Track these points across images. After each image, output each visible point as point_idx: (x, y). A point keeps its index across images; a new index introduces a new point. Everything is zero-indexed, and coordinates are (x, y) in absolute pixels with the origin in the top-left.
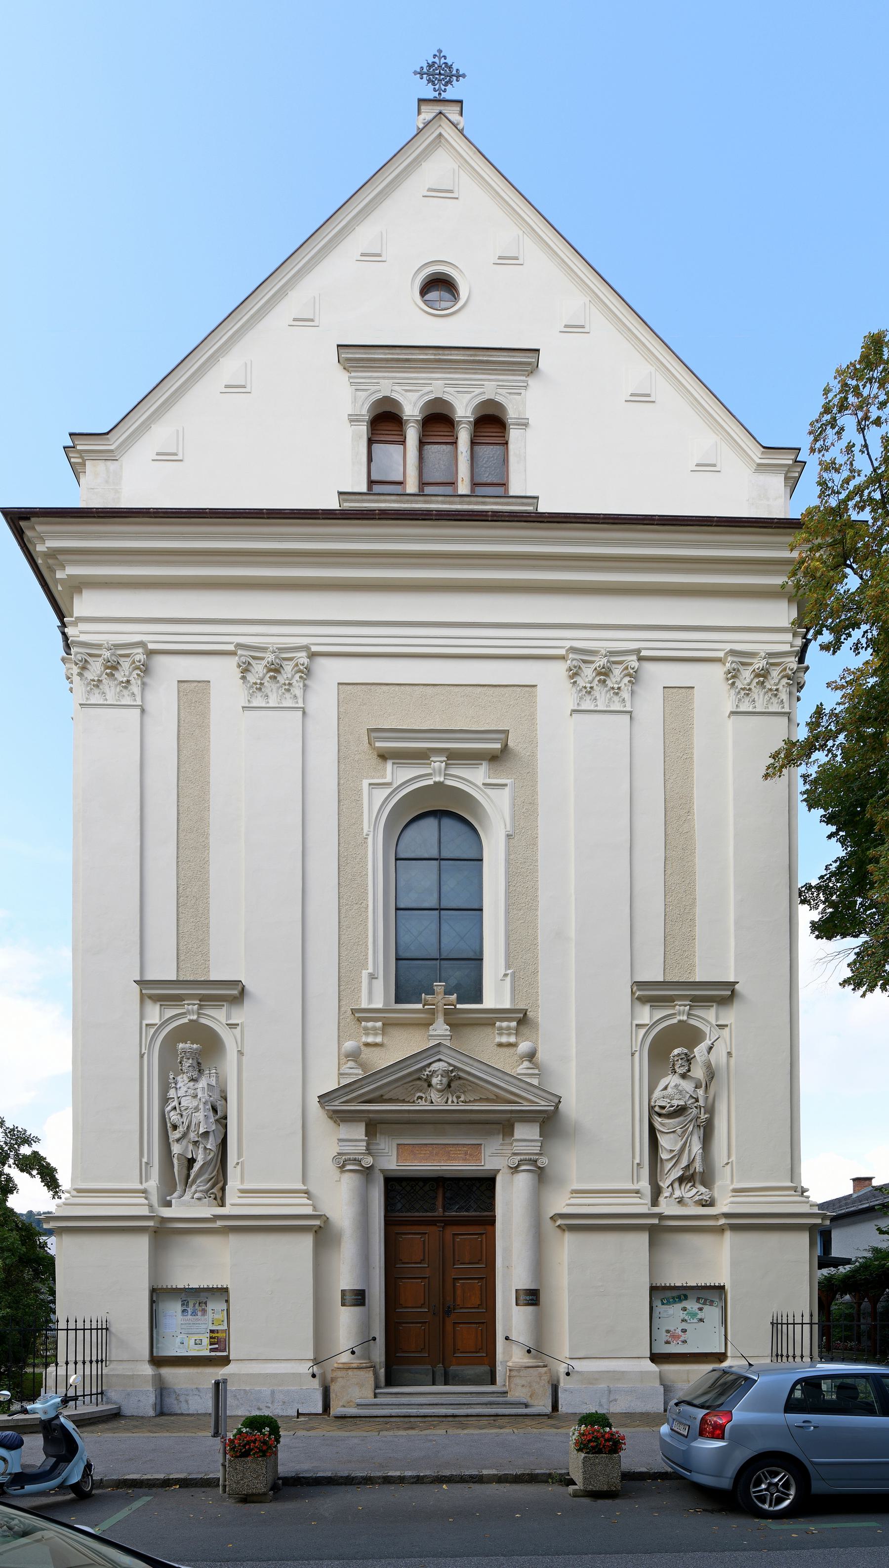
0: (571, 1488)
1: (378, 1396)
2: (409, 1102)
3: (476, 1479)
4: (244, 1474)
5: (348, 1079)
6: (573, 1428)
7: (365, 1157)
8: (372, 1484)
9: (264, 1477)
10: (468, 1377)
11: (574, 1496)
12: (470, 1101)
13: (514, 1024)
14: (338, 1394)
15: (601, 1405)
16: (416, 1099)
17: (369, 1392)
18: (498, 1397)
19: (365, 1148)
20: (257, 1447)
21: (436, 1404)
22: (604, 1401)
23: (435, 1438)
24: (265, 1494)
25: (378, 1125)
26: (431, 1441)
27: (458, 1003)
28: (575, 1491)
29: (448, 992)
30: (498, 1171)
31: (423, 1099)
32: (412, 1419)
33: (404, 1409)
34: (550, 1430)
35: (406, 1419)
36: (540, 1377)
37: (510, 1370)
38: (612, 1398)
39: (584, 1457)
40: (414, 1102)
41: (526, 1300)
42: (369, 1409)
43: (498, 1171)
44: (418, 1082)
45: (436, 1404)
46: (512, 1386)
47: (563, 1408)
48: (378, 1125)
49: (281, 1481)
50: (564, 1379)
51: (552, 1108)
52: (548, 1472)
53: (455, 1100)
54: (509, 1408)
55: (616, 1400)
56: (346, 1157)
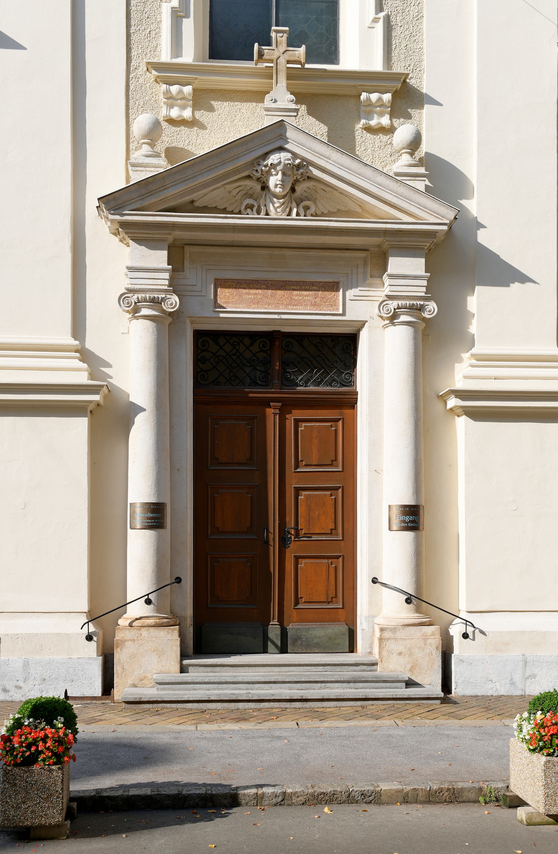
0: (521, 813)
1: (190, 669)
2: (232, 212)
3: (371, 798)
4: (27, 793)
5: (143, 173)
6: (518, 716)
7: (168, 296)
8: (214, 807)
9: (58, 797)
10: (316, 641)
11: (529, 824)
12: (323, 215)
13: (387, 97)
14: (126, 667)
15: (513, 683)
16: (243, 208)
17: (173, 663)
18: (364, 671)
19: (167, 282)
20: (48, 749)
21: (275, 682)
22: (517, 677)
23: (285, 734)
24: (58, 826)
25: (187, 248)
26: (279, 738)
27: (308, 61)
28: (530, 816)
29: (292, 42)
30: (363, 324)
31: (255, 209)
32: (241, 705)
33: (227, 689)
34: (449, 721)
35: (232, 705)
36: (425, 640)
37: (382, 630)
38: (528, 674)
39: (546, 763)
40: (240, 213)
41: (404, 522)
42: (174, 690)
43: (363, 324)
44: (248, 183)
45: (275, 682)
46: (385, 654)
47: (457, 689)
48: (187, 248)
49: (76, 804)
50: (460, 643)
51: (445, 228)
52: (476, 785)
53: (302, 212)
54: (382, 688)
55: (534, 676)
56: (140, 296)
